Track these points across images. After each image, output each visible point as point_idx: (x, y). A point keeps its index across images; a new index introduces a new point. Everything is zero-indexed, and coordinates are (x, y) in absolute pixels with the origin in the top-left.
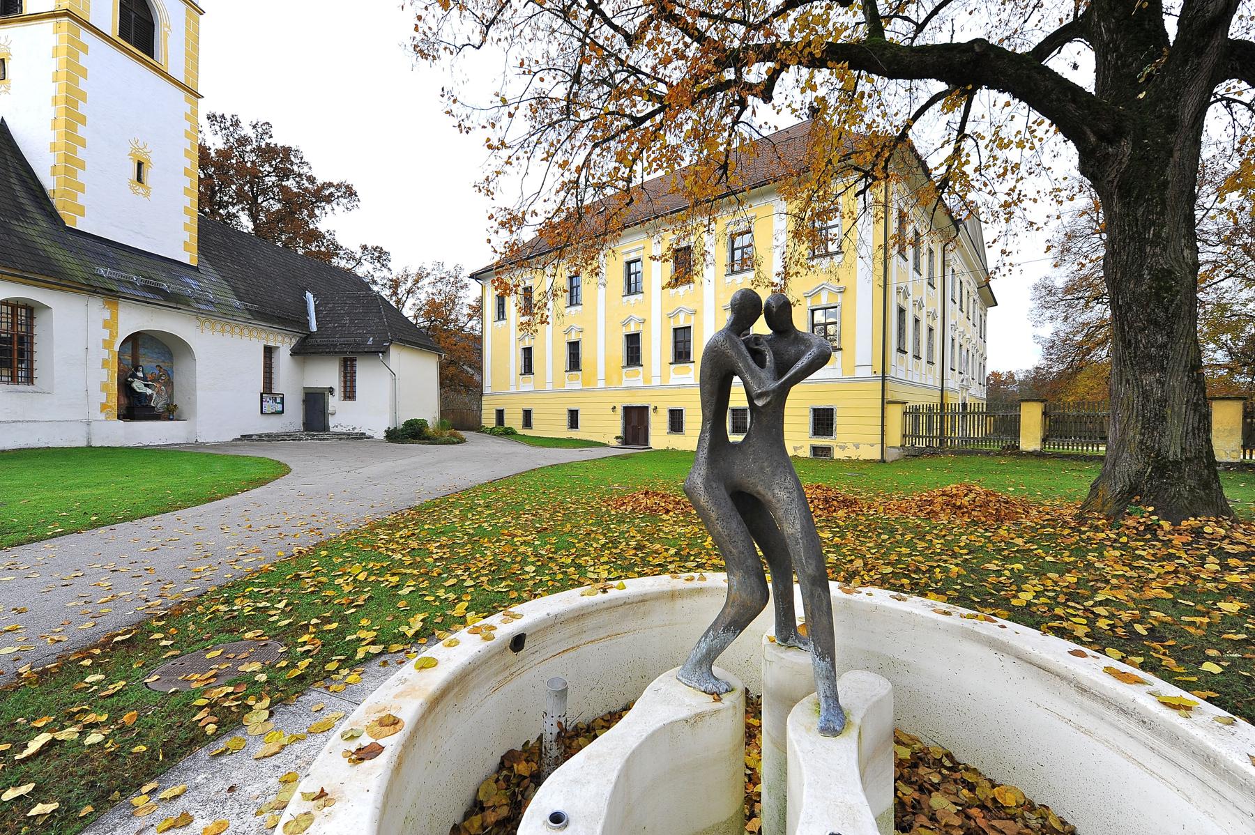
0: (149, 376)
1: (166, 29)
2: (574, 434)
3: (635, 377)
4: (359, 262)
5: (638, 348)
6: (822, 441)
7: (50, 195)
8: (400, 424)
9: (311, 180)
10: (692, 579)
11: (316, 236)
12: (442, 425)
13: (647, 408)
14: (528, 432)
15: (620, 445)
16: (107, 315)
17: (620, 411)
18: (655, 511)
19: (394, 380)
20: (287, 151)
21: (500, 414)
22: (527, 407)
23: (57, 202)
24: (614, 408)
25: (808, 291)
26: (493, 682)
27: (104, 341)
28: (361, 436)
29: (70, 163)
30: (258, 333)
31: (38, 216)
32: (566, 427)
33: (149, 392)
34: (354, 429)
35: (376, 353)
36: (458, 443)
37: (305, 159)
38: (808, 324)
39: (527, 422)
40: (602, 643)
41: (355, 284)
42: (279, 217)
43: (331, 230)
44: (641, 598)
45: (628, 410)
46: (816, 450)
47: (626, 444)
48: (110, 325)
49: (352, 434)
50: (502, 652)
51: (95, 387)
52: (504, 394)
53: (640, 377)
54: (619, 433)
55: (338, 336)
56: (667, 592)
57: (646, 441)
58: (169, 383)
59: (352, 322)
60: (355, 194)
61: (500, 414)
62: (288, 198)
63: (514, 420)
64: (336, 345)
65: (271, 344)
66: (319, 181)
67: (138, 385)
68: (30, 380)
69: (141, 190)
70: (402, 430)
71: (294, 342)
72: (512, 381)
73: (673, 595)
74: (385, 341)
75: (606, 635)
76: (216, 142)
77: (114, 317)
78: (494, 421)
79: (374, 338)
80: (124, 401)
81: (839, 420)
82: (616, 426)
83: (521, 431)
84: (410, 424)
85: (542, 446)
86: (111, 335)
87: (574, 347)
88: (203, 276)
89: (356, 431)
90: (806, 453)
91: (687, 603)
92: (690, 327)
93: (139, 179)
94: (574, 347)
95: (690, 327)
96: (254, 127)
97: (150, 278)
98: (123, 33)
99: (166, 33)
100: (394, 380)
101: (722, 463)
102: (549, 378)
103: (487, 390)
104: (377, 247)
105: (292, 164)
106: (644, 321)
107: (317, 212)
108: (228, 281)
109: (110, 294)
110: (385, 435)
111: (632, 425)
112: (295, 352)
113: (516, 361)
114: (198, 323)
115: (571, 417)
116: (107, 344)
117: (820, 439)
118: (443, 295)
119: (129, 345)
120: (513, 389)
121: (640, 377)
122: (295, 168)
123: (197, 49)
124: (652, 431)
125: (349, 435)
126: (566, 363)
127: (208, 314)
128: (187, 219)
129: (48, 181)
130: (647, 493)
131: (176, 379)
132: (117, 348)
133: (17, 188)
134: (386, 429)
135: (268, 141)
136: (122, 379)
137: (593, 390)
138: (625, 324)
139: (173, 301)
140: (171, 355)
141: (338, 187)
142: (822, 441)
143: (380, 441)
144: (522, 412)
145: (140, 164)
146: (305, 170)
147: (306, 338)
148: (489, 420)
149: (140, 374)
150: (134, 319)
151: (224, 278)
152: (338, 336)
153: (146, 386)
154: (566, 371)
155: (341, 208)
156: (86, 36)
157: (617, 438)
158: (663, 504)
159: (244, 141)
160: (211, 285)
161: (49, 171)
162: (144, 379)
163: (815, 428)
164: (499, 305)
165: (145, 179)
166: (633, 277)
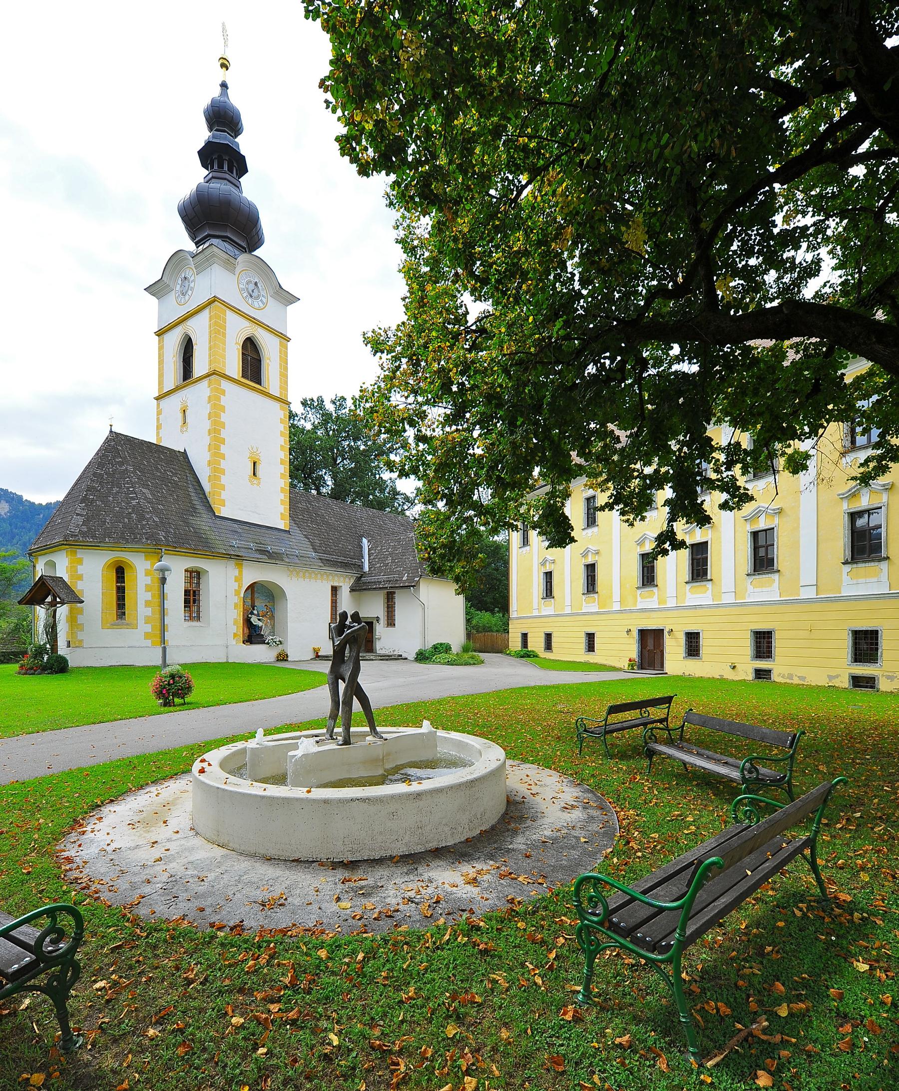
0: (260, 613)
1: (268, 361)
2: (591, 658)
3: (649, 599)
5: (705, 560)
6: (763, 664)
8: (429, 645)
12: (465, 649)
13: (661, 631)
16: (237, 572)
17: (635, 634)
21: (525, 636)
22: (548, 631)
25: (843, 492)
27: (235, 590)
28: (399, 658)
29: (217, 472)
30: (328, 576)
32: (583, 651)
33: (260, 624)
34: (394, 651)
36: (474, 664)
38: (844, 529)
39: (548, 646)
41: (402, 525)
46: (858, 682)
47: (642, 669)
48: (238, 579)
53: (655, 598)
55: (382, 574)
58: (272, 617)
61: (525, 636)
62: (354, 455)
63: (536, 644)
65: (336, 584)
67: (254, 620)
68: (198, 618)
69: (255, 482)
71: (352, 581)
72: (535, 606)
77: (241, 574)
78: (520, 644)
79: (409, 574)
80: (246, 631)
81: (885, 644)
82: (633, 650)
83: (543, 654)
86: (239, 586)
87: (591, 568)
88: (293, 537)
89: (395, 653)
90: (751, 676)
92: (707, 542)
93: (254, 474)
94: (591, 568)
95: (707, 542)
97: (261, 543)
98: (244, 376)
99: (268, 364)
108: (308, 538)
112: (353, 590)
116: (237, 593)
117: (861, 667)
120: (535, 613)
123: (286, 369)
124: (667, 656)
126: (584, 586)
128: (282, 496)
129: (207, 486)
131: (277, 615)
133: (193, 494)
136: (246, 617)
139: (272, 557)
142: (763, 664)
144: (543, 635)
145: (254, 463)
147: (361, 577)
148: (515, 643)
149: (255, 612)
150: (252, 574)
152: (382, 574)
153: (259, 620)
154: (583, 594)
156: (225, 385)
162: (258, 615)
163: (856, 654)
165: (257, 473)
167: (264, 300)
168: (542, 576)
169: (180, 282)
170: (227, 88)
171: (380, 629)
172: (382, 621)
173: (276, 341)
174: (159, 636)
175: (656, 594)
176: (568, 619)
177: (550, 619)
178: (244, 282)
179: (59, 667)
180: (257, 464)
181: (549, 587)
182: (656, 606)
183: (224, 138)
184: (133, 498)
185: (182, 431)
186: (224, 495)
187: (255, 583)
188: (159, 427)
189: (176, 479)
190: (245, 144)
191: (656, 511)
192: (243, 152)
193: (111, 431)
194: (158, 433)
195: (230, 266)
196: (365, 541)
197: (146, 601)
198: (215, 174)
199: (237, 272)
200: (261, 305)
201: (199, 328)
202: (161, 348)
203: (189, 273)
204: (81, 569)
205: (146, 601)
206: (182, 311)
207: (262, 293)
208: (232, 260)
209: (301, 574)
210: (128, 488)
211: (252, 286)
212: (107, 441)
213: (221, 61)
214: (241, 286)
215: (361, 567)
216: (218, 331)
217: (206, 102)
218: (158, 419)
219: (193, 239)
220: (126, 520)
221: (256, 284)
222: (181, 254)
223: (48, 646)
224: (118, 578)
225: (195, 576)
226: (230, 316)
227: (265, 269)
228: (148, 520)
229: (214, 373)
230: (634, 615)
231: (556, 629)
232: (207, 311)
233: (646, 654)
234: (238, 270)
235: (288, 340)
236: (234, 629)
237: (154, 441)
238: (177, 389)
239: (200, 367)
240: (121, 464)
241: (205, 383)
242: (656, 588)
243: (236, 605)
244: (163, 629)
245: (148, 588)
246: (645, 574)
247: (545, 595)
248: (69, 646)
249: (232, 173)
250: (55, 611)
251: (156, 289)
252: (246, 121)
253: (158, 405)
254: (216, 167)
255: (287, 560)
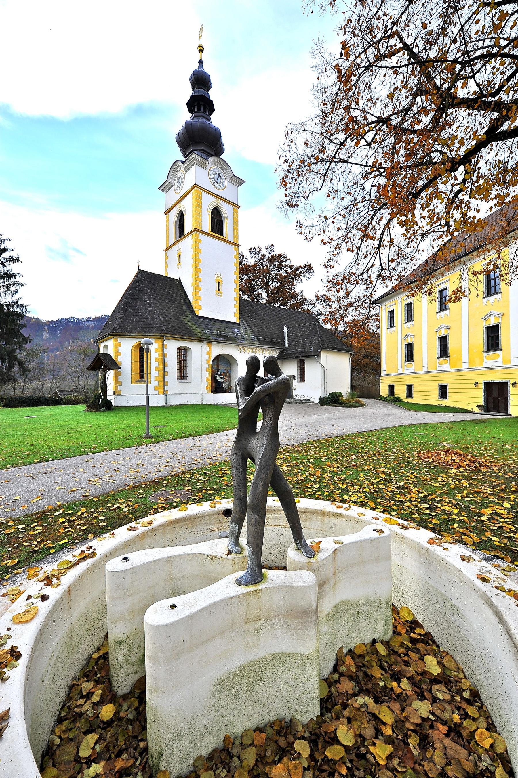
2: (444, 403)
4: (314, 305)
7: (192, 303)
9: (291, 267)
10: (341, 507)
11: (294, 296)
12: (352, 396)
13: (506, 383)
14: (410, 400)
15: (481, 412)
17: (482, 386)
18: (450, 465)
19: (324, 370)
20: (280, 255)
21: (392, 388)
22: (410, 383)
23: (194, 306)
24: (476, 384)
26: (212, 526)
28: (307, 401)
31: (188, 313)
32: (437, 398)
33: (222, 380)
34: (304, 397)
35: (314, 356)
36: (359, 406)
37: (288, 258)
39: (443, 391)
40: (280, 528)
41: (309, 318)
42: (279, 289)
43: (301, 290)
44: (304, 510)
45: (489, 386)
47: (485, 412)
48: (209, 353)
49: (303, 400)
50: (217, 514)
51: (204, 379)
52: (394, 375)
53: (500, 359)
54: (481, 402)
56: (320, 511)
57: (506, 409)
59: (303, 340)
60: (312, 269)
61: (392, 388)
62: (280, 278)
63: (401, 393)
64: (295, 353)
66: (295, 267)
67: (219, 378)
68: (186, 378)
70: (327, 398)
71: (278, 353)
72: (400, 367)
73: (324, 514)
74: (318, 349)
75: (282, 524)
76: (250, 261)
78: (388, 393)
80: (214, 385)
82: (480, 398)
83: (406, 400)
84: (332, 395)
85: (416, 410)
89: (305, 398)
91: (332, 521)
93: (219, 290)
96: (267, 249)
97: (222, 331)
100: (324, 370)
101: (244, 441)
102: (425, 363)
103: (383, 373)
104: (324, 295)
105: (283, 262)
106: (503, 315)
107: (295, 283)
109: (208, 340)
110: (318, 401)
111: (493, 396)
113: (402, 353)
114: (239, 349)
115: (442, 391)
116: (208, 361)
118: (362, 316)
119: (216, 361)
120: (400, 372)
121: (500, 359)
122: (284, 263)
125: (301, 400)
126: (437, 352)
127: (243, 344)
128: (235, 302)
130: (447, 451)
132: (211, 363)
134: (319, 397)
135: (272, 254)
137: (459, 370)
138: (438, 330)
139: (227, 340)
140: (230, 364)
141: (303, 268)
143: (316, 404)
144: (406, 387)
145: (219, 283)
146: (288, 263)
147: (283, 351)
148: (384, 392)
149: (219, 373)
150: (217, 350)
151: (250, 327)
153: (221, 378)
154: (437, 358)
155: (306, 278)
156: (202, 236)
157: (478, 406)
158: (458, 461)
159: (263, 257)
160: (245, 332)
161: (191, 294)
162: (221, 375)
164: (391, 318)
166: (492, 282)
167: (224, 184)
168: (404, 348)
169: (177, 180)
170: (203, 63)
171: (296, 383)
172: (296, 378)
173: (231, 208)
174: (162, 388)
175: (501, 356)
176: (425, 375)
177: (411, 376)
178: (212, 174)
179: (108, 406)
180: (220, 284)
181: (409, 354)
182: (500, 364)
183: (201, 92)
184: (149, 307)
185: (178, 268)
186: (201, 303)
187: (219, 355)
188: (166, 267)
189: (174, 295)
190: (213, 94)
191: (500, 294)
192: (211, 99)
193: (139, 269)
194: (166, 270)
195: (204, 165)
196: (286, 328)
197: (155, 367)
198: (196, 114)
199: (208, 169)
200: (222, 187)
201: (187, 205)
202: (167, 221)
203: (181, 174)
204: (120, 349)
205: (155, 367)
206: (177, 197)
207: (223, 180)
208: (205, 161)
209: (246, 349)
210: (147, 301)
211: (217, 176)
212: (137, 275)
213: (199, 48)
214: (211, 177)
215: (283, 343)
216: (198, 204)
217: (190, 73)
218: (166, 262)
219: (184, 155)
220: (145, 320)
221: (219, 175)
222: (177, 164)
223: (102, 394)
224: (140, 353)
225: (183, 352)
226: (204, 194)
227: (225, 165)
228: (157, 319)
229: (195, 230)
230: (481, 372)
231: (416, 382)
232: (191, 194)
233: (491, 399)
234: (209, 166)
235: (239, 207)
236: (206, 384)
237: (164, 275)
238: (176, 242)
239: (187, 228)
240: (143, 287)
241: (190, 237)
242: (501, 352)
243: (207, 369)
244: (165, 384)
245: (156, 359)
246: (490, 342)
247: (407, 360)
248: (114, 394)
249: (205, 112)
250: (106, 374)
251: (164, 187)
252: (213, 80)
253: (166, 254)
254: (196, 110)
255: (238, 341)
